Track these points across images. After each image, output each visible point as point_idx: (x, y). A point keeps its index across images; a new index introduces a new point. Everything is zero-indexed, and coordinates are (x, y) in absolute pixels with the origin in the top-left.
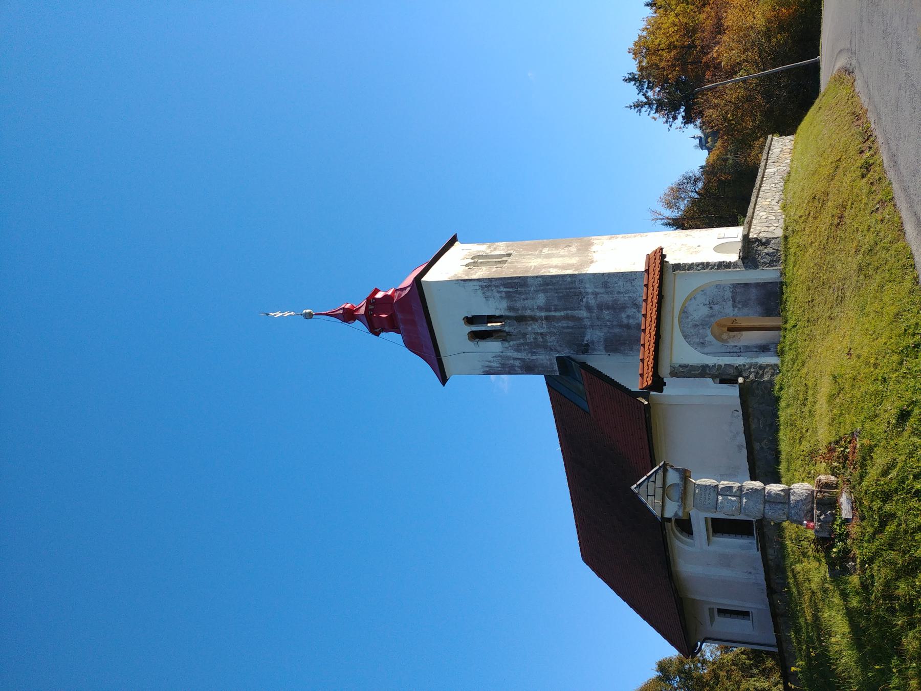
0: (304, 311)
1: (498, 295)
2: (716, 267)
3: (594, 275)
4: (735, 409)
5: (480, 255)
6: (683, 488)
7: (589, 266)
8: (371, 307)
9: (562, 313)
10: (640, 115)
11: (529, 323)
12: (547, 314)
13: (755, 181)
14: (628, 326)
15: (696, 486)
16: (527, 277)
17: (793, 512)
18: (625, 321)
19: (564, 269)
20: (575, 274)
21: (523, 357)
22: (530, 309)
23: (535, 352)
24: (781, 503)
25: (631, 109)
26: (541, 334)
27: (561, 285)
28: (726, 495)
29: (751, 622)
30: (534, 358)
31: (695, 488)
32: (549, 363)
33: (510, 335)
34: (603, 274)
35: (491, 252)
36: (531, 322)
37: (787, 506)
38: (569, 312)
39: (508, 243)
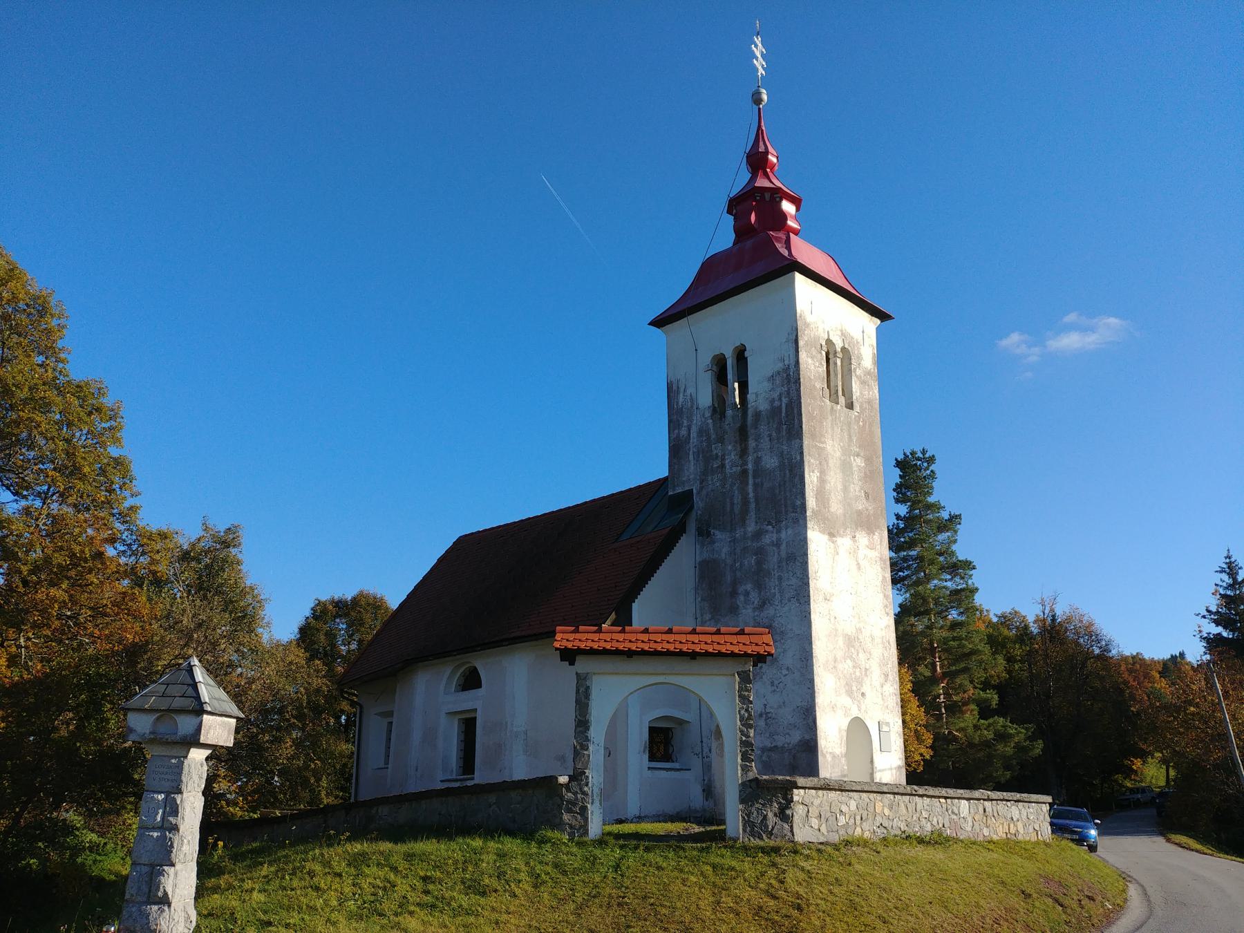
0: (764, 91)
1: (776, 395)
2: (744, 738)
3: (804, 541)
4: (612, 753)
5: (851, 360)
6: (169, 740)
7: (822, 532)
8: (767, 196)
9: (751, 495)
10: (1216, 571)
11: (738, 445)
12: (751, 472)
13: (932, 786)
14: (734, 594)
15: (182, 759)
16: (801, 439)
17: (134, 909)
18: (741, 589)
19: (817, 495)
20: (806, 512)
21: (691, 441)
22: (757, 446)
23: (699, 457)
24: (150, 891)
25: (1226, 558)
26: (723, 466)
27: (791, 491)
28: (165, 806)
29: (383, 766)
30: (691, 457)
31: (179, 757)
32: (684, 479)
33: (721, 419)
34: (805, 554)
35: (859, 377)
36: (739, 449)
37: (145, 899)
38: (753, 506)
39: (878, 401)
